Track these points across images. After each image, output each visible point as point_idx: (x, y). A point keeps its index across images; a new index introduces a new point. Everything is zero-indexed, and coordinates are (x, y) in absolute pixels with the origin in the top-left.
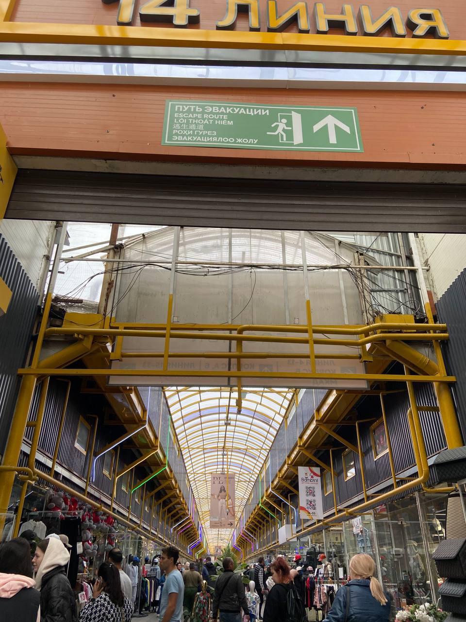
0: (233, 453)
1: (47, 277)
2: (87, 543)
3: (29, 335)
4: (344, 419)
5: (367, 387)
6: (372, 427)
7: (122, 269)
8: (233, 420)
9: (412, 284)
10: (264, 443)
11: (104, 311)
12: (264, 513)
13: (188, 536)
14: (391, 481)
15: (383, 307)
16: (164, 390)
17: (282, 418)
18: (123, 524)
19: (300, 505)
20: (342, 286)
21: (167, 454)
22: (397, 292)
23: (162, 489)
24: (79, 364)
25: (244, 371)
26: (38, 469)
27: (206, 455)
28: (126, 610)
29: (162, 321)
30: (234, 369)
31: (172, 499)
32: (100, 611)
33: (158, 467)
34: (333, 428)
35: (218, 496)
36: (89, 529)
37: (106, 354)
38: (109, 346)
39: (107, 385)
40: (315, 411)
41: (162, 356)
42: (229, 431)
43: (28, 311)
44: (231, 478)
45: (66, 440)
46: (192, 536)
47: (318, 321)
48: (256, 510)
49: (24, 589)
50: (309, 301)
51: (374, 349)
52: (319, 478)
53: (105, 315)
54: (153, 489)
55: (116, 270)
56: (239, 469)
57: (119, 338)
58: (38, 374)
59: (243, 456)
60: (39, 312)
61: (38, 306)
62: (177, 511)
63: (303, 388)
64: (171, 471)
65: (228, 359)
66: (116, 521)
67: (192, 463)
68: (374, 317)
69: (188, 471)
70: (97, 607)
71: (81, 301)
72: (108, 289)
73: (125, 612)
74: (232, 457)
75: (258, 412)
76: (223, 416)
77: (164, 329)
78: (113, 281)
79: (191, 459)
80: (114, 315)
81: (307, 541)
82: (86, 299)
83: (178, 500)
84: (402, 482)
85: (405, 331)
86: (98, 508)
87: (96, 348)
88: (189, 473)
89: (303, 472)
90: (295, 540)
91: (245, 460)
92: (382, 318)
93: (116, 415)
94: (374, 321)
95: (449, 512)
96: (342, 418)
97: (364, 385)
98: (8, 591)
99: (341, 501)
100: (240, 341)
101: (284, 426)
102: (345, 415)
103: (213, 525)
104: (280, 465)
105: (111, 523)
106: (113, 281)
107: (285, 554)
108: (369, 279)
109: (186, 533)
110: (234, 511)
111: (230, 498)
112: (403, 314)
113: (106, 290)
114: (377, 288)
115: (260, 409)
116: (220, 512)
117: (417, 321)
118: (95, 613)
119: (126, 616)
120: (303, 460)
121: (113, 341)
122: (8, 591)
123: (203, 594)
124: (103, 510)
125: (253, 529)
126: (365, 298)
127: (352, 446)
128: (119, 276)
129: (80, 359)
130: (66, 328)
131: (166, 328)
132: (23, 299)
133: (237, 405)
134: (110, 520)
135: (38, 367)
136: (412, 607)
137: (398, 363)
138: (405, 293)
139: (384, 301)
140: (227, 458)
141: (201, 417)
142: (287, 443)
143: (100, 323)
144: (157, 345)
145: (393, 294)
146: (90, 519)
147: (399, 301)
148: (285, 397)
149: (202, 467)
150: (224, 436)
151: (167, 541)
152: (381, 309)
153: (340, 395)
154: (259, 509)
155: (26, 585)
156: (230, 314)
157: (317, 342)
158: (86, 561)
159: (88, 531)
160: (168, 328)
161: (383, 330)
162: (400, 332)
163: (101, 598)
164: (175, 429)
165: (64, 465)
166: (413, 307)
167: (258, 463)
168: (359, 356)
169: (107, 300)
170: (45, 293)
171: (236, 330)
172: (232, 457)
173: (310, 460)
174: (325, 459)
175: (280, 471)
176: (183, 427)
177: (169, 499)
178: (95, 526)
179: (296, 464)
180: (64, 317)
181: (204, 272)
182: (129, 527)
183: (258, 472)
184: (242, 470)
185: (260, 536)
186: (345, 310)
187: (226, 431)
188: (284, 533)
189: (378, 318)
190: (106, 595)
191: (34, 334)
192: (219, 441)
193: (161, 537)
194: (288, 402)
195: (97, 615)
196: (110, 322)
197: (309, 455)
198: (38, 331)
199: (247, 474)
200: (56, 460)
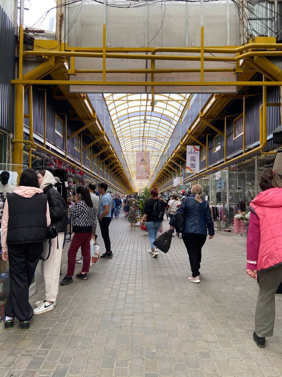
0: (149, 140)
1: (17, 12)
2: (70, 183)
3: (13, 57)
4: (218, 116)
5: (236, 91)
6: (235, 120)
7: (69, 4)
8: (149, 120)
9: (279, 13)
10: (168, 131)
11: (60, 38)
12: (166, 172)
13: (124, 183)
14: (242, 151)
15: (256, 32)
16: (105, 100)
17: (179, 118)
18: (89, 175)
19: (187, 166)
20: (228, 15)
21: (110, 140)
22: (267, 20)
23: (109, 159)
24: (48, 77)
25: (156, 82)
26: (36, 142)
27: (133, 141)
28: (94, 209)
29: (98, 45)
30: (149, 81)
31: (115, 165)
32: (81, 209)
33: (110, 154)
34: (210, 122)
35: (140, 163)
36: (70, 177)
37: (65, 70)
38: (66, 64)
39: (68, 92)
40: (200, 111)
41: (102, 72)
42: (146, 127)
43: (9, 38)
44: (148, 154)
45: (50, 129)
46: (127, 184)
47: (209, 44)
48: (162, 171)
49: (37, 194)
50: (203, 27)
51: (245, 64)
52: (199, 152)
53: (60, 41)
54: (104, 159)
55: (64, 5)
56: (152, 149)
57: (72, 58)
58: (25, 84)
59: (154, 142)
60: (17, 42)
61: (15, 35)
62: (118, 171)
63: (196, 93)
64: (113, 149)
65: (145, 60)
66: (85, 174)
67: (125, 146)
68: (248, 39)
69: (123, 150)
70: (79, 207)
71: (42, 32)
72: (60, 21)
73: (93, 209)
74: (148, 142)
75: (164, 115)
76: (142, 118)
77: (102, 51)
78: (63, 14)
79: (124, 143)
80: (66, 42)
81: (189, 185)
82: (47, 30)
83: (118, 165)
84: (250, 149)
85: (268, 49)
86: (74, 166)
87: (57, 66)
88: (124, 151)
89: (189, 148)
90: (182, 184)
91: (155, 144)
92: (253, 40)
93: (77, 115)
94: (248, 43)
95: (274, 168)
96: (217, 115)
97: (234, 90)
98: (28, 195)
99: (210, 164)
100: (153, 59)
101: (180, 123)
102: (219, 113)
103: (138, 178)
104: (175, 147)
105: (82, 175)
106: (63, 14)
107: (176, 191)
108: (248, 9)
109: (123, 182)
110: (149, 171)
111: (147, 164)
112: (269, 36)
113: (59, 22)
114: (253, 17)
115: (165, 112)
116: (141, 172)
117: (277, 42)
118: (78, 209)
119: (94, 212)
120: (190, 142)
121: (68, 61)
122: (28, 195)
123: (133, 207)
124: (77, 168)
125: (160, 180)
126: (243, 24)
127: (221, 132)
128: (67, 9)
129: (49, 74)
130: (36, 51)
131: (102, 51)
132: (4, 30)
133: (151, 106)
134: (81, 173)
135: (23, 79)
136: (244, 213)
137: (260, 73)
138: (272, 21)
139: (257, 27)
140: (145, 143)
141: (129, 118)
142: (181, 133)
143: (58, 47)
144: (96, 64)
145: (264, 21)
146: (70, 172)
147: (267, 26)
148: (181, 104)
149: (131, 148)
150: (143, 130)
151: (113, 185)
152: (254, 33)
153: (218, 99)
154: (163, 170)
155: (38, 192)
156: (146, 39)
157: (206, 59)
158: (71, 192)
159: (70, 178)
160: (104, 51)
161: (253, 49)
162: (265, 50)
163: (80, 203)
164: (113, 126)
165: (51, 142)
166: (277, 32)
167: (163, 146)
168: (234, 69)
169: (60, 30)
170: (19, 26)
171: (150, 51)
172: (148, 142)
173: (195, 142)
174: (203, 141)
175: (176, 149)
176: (118, 124)
177: (113, 164)
178: (74, 175)
179: (185, 145)
180: (33, 43)
181: (126, 5)
182: (92, 177)
183: (163, 151)
184: (154, 150)
185: (163, 184)
186: (228, 34)
187: (144, 130)
188: (177, 181)
189: (251, 40)
190: (83, 202)
191: (16, 56)
192: (140, 133)
193: (110, 183)
194: (181, 113)
195: (79, 210)
196: (65, 47)
197: (194, 139)
198: (18, 54)
199: (156, 152)
200: (46, 139)
